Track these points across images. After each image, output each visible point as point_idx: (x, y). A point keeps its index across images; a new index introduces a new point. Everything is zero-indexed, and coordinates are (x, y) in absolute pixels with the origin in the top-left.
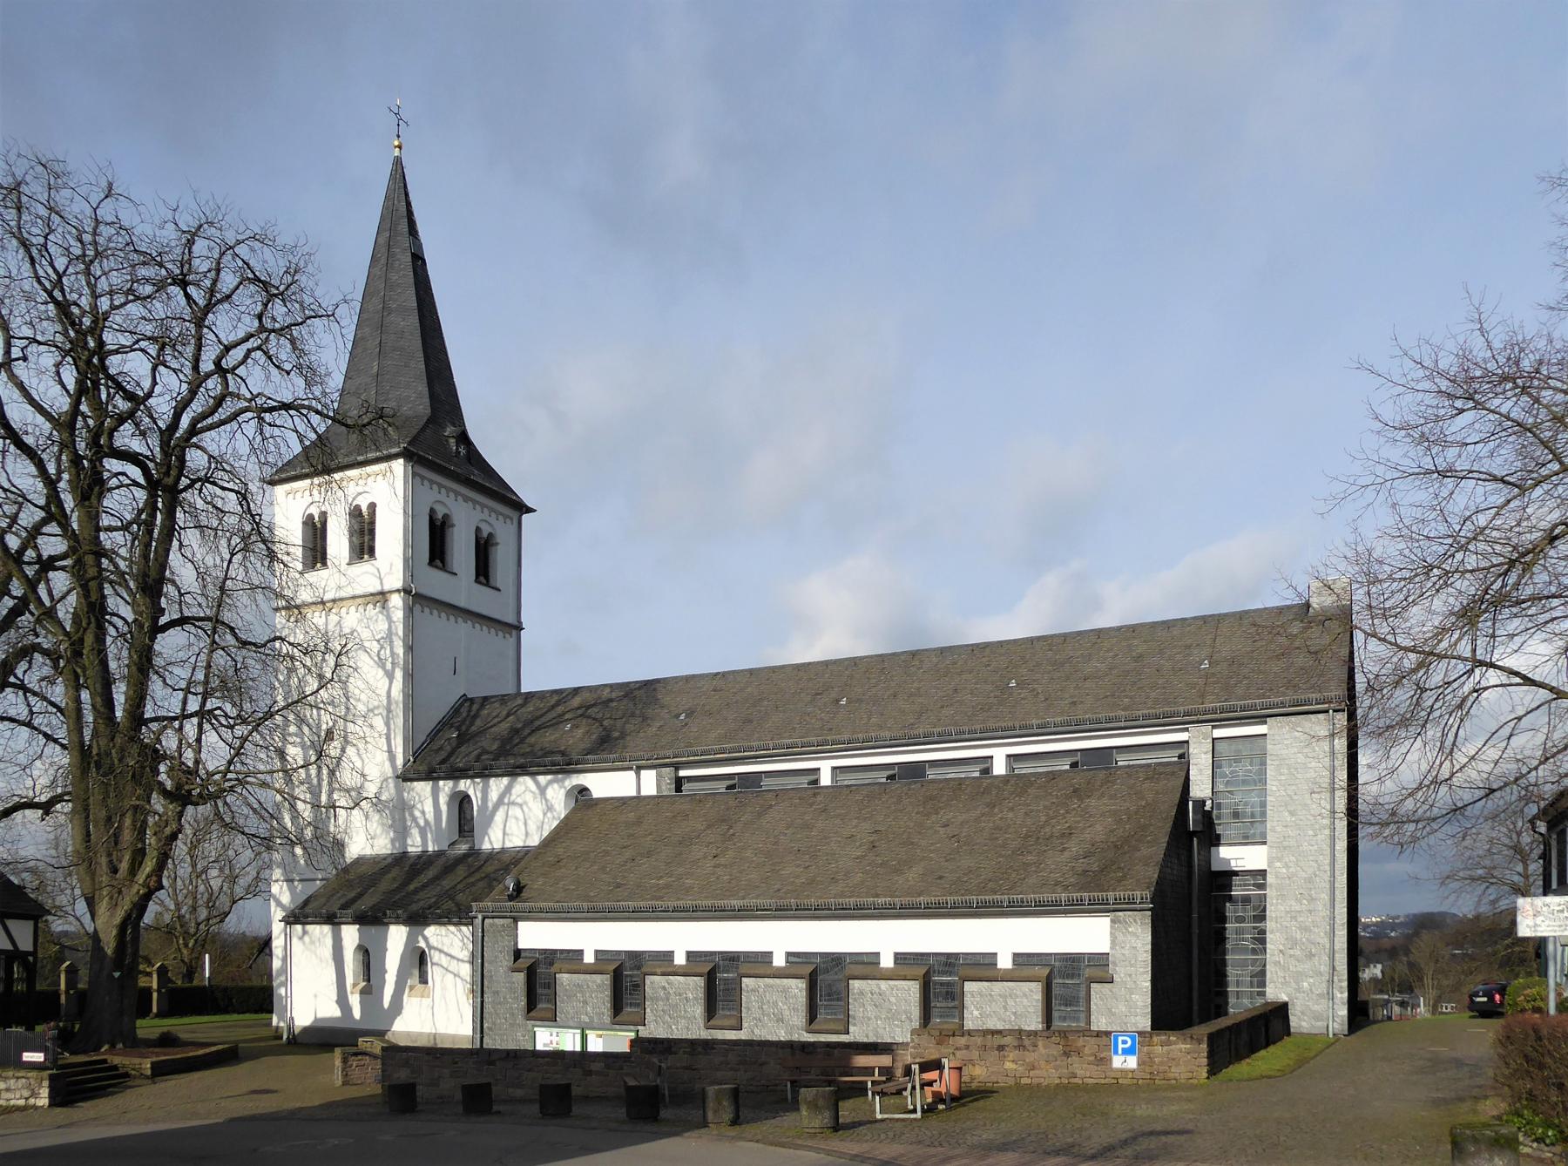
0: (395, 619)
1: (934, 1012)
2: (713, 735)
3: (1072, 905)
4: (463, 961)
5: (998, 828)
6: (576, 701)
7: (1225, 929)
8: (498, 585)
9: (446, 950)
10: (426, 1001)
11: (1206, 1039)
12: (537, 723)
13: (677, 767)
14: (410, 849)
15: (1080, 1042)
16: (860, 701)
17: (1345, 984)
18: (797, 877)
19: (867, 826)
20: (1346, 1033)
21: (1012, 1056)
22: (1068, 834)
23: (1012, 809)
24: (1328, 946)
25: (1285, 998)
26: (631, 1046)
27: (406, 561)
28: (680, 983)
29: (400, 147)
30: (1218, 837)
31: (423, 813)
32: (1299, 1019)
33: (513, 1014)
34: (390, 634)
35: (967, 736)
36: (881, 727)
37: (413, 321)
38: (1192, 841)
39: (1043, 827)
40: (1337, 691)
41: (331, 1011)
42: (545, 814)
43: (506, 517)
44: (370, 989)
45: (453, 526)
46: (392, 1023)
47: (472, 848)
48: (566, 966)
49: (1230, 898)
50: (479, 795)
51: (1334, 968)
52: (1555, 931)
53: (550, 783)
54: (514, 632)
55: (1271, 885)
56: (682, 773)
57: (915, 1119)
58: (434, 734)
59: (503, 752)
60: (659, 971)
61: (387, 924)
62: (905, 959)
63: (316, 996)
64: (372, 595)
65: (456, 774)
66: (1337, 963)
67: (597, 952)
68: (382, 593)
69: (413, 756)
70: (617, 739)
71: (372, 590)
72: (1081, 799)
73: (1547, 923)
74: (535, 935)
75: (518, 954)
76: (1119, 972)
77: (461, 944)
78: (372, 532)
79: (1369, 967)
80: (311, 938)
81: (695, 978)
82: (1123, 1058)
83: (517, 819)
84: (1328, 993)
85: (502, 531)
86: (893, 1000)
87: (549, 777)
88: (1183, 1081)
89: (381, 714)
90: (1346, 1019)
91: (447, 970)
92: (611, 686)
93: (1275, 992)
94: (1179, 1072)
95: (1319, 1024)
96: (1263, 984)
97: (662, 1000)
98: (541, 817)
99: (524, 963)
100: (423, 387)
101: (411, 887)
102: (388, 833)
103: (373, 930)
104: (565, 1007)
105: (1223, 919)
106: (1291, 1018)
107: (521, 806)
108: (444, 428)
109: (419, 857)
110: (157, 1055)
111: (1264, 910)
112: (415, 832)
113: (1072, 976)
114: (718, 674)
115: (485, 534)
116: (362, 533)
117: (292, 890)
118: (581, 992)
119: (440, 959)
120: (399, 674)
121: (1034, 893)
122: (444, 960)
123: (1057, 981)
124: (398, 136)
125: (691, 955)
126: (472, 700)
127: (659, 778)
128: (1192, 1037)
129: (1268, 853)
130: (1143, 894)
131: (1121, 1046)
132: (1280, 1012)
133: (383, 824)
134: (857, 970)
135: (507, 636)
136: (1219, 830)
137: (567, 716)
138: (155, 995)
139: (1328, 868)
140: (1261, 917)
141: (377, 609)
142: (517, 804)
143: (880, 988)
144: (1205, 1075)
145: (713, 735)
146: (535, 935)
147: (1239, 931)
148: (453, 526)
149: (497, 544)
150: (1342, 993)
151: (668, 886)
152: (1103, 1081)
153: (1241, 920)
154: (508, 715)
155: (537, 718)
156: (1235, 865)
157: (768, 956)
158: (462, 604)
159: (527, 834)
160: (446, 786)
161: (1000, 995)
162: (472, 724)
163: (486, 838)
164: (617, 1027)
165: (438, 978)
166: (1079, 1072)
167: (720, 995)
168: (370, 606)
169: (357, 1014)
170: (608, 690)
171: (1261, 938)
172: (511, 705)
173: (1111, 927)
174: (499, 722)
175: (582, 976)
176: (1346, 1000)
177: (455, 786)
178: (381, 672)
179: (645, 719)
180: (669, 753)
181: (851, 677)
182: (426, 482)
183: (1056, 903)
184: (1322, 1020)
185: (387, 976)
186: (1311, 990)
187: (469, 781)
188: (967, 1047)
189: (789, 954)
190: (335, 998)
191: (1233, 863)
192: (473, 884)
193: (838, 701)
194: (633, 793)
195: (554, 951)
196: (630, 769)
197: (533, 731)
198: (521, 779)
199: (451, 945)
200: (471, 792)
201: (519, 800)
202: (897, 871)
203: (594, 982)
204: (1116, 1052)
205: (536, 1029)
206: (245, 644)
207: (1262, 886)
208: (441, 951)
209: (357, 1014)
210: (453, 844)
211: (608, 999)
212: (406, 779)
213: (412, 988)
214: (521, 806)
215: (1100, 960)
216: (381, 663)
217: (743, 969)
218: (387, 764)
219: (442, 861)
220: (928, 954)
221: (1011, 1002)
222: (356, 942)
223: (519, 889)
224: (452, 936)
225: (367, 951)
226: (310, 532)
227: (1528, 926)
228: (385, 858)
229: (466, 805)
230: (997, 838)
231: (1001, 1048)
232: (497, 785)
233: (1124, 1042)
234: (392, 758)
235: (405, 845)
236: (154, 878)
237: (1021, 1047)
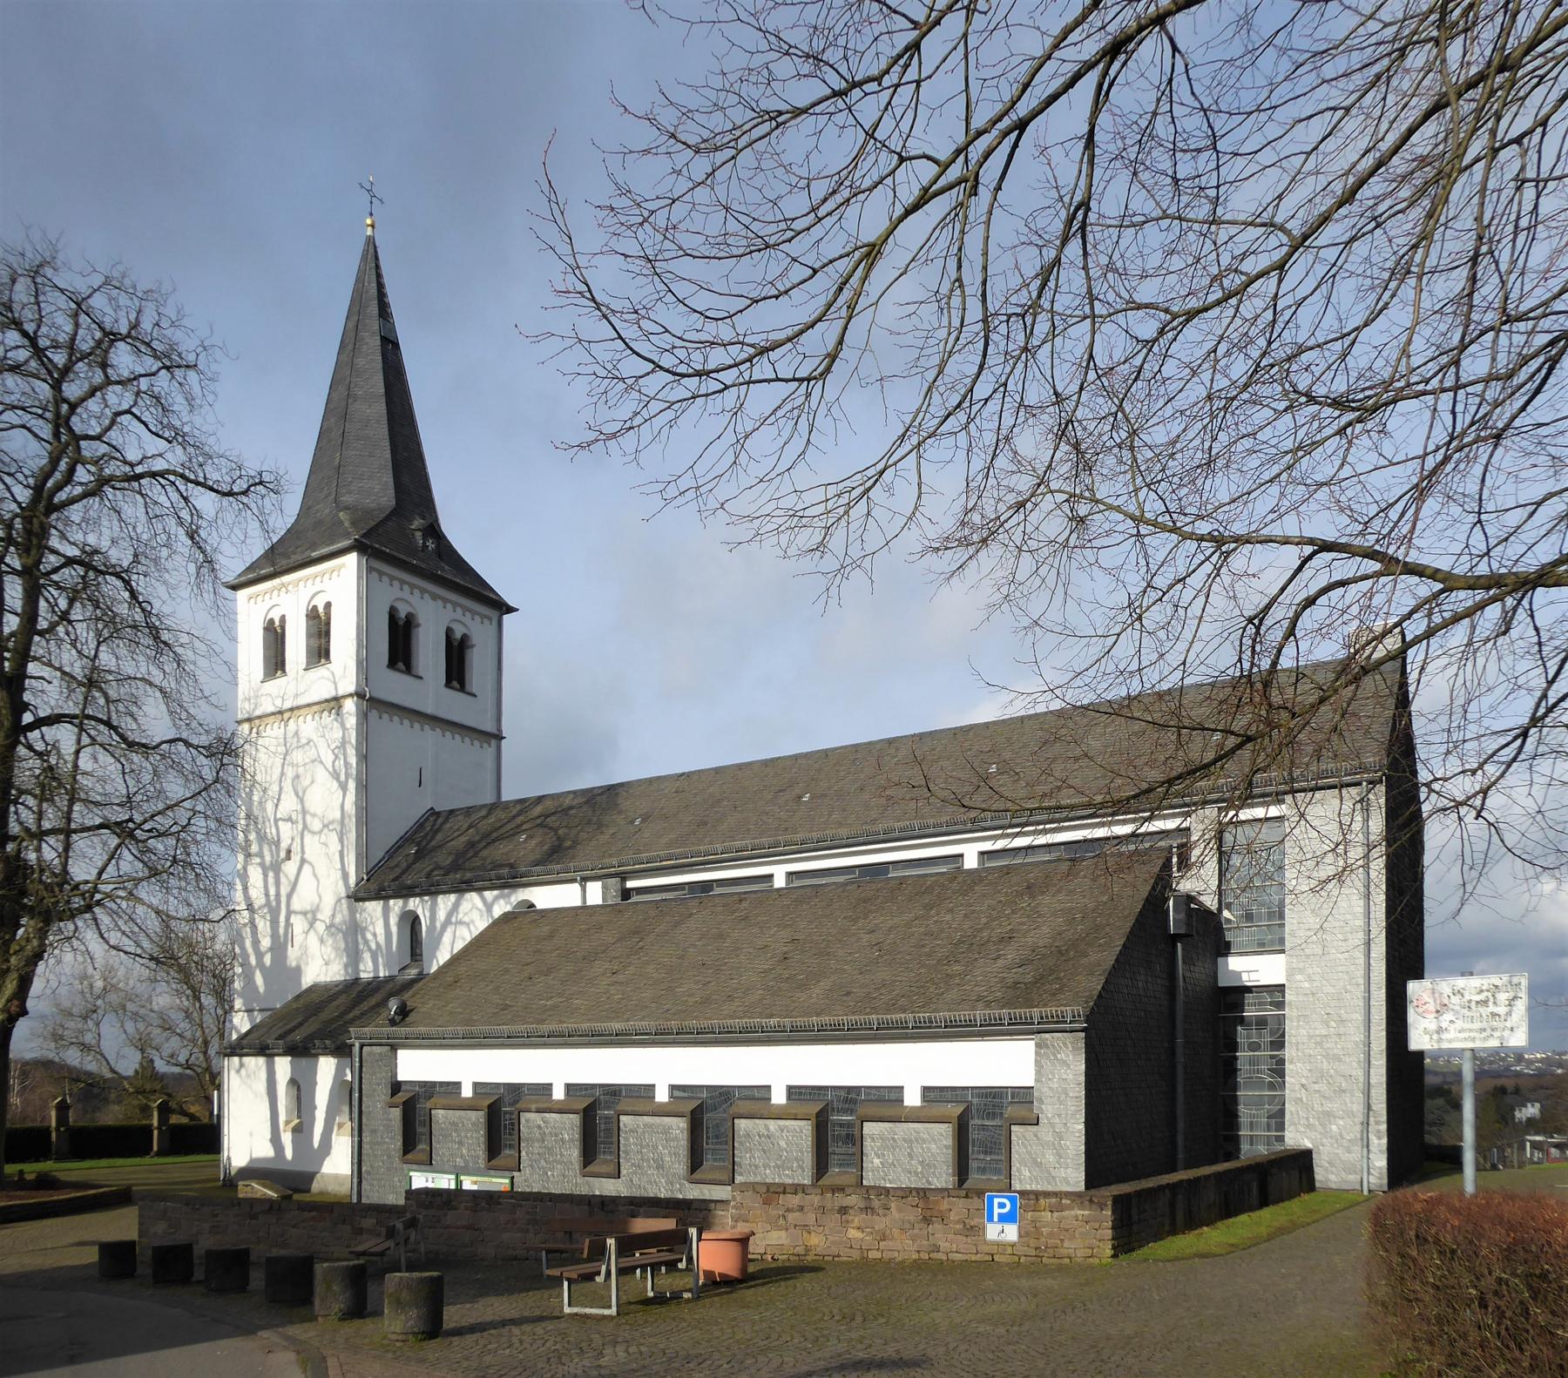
0: (348, 726)
1: (833, 1159)
2: (664, 840)
3: (990, 1025)
5: (930, 934)
6: (538, 810)
7: (1236, 1058)
8: (474, 691)
11: (1110, 1203)
12: (495, 835)
13: (624, 877)
14: (363, 975)
15: (945, 1205)
16: (824, 796)
17: (1384, 1127)
18: (692, 995)
19: (785, 934)
20: (1386, 1189)
21: (857, 1220)
22: (1009, 938)
23: (951, 911)
24: (1361, 1080)
25: (1309, 1145)
26: (406, 1198)
27: (359, 663)
28: (555, 1121)
29: (373, 226)
30: (1228, 945)
31: (375, 935)
32: (1326, 1170)
33: (389, 1156)
34: (344, 743)
35: (931, 830)
36: (840, 825)
37: (380, 408)
38: (1175, 947)
39: (981, 930)
40: (1374, 756)
41: (265, 1151)
43: (483, 617)
44: (301, 1131)
45: (418, 625)
47: (421, 973)
48: (445, 1101)
49: (1242, 1020)
50: (428, 914)
51: (1369, 1108)
52: (1473, 1040)
53: (496, 898)
54: (493, 742)
55: (1290, 1003)
56: (630, 884)
57: (604, 1317)
58: (392, 852)
59: (455, 867)
60: (533, 1107)
61: (316, 1056)
62: (800, 1093)
63: (251, 1134)
64: (327, 701)
65: (405, 892)
66: (1373, 1101)
67: (476, 1085)
68: (336, 699)
70: (569, 848)
71: (328, 696)
72: (1033, 897)
73: (1459, 1024)
74: (415, 1065)
75: (396, 1087)
76: (1047, 1110)
78: (328, 633)
79: (1526, 1106)
81: (571, 1116)
82: (999, 1227)
84: (1362, 1139)
85: (476, 629)
86: (783, 1144)
87: (496, 892)
88: (1079, 1260)
90: (1385, 1171)
92: (574, 792)
93: (1296, 1137)
94: (1075, 1248)
95: (1351, 1177)
96: (1281, 1127)
97: (538, 1140)
99: (402, 1097)
100: (388, 478)
103: (304, 1062)
104: (441, 1150)
105: (1234, 1047)
106: (1316, 1169)
107: (468, 925)
108: (410, 521)
109: (369, 983)
110: (21, 1198)
111: (1283, 1035)
112: (367, 956)
113: (992, 1116)
114: (683, 774)
115: (458, 635)
116: (320, 635)
117: (251, 1019)
118: (456, 1131)
120: (352, 785)
121: (949, 1010)
123: (975, 1122)
124: (371, 214)
125: (792, 1091)
126: (438, 814)
127: (605, 888)
128: (1091, 1201)
129: (1287, 962)
130: (1074, 1010)
131: (997, 1211)
132: (1302, 1161)
134: (743, 1106)
135: (485, 745)
136: (1229, 937)
137: (524, 827)
138: (156, 1133)
139: (1361, 981)
140: (1279, 1044)
141: (333, 717)
143: (768, 1130)
144: (1109, 1252)
145: (664, 840)
146: (415, 1065)
147: (1253, 1062)
148: (418, 625)
149: (473, 646)
150: (1379, 1138)
151: (555, 1007)
152: (974, 1258)
153: (1255, 1047)
154: (470, 827)
155: (496, 829)
156: (1248, 980)
157: (457, 1085)
158: (429, 710)
160: (396, 905)
161: (904, 1140)
162: (433, 838)
164: (492, 1172)
166: (944, 1245)
167: (601, 1137)
168: (326, 714)
169: (289, 1154)
170: (571, 796)
171: (1279, 1070)
172: (475, 817)
173: (1036, 1053)
175: (458, 1113)
176: (1385, 1147)
177: (405, 904)
178: (335, 784)
179: (600, 825)
180: (615, 862)
181: (819, 770)
182: (385, 579)
183: (971, 1023)
184: (1356, 1173)
186: (1341, 1135)
188: (801, 1209)
189: (673, 1088)
190: (269, 1137)
191: (1245, 977)
193: (800, 797)
194: (578, 903)
195: (433, 1084)
196: (573, 881)
197: (489, 844)
200: (420, 912)
201: (466, 919)
202: (803, 986)
203: (470, 1119)
204: (991, 1219)
205: (411, 1174)
206: (131, 745)
207: (1280, 1005)
209: (289, 1154)
210: (404, 968)
211: (482, 1139)
212: (358, 900)
213: (340, 1126)
215: (1023, 1095)
216: (335, 775)
217: (862, 1110)
218: (341, 883)
219: (390, 986)
220: (826, 1088)
221: (917, 1149)
222: (288, 1076)
223: (404, 1012)
226: (272, 638)
227: (1426, 1031)
228: (337, 984)
230: (923, 946)
231: (843, 1210)
232: (445, 902)
233: (1002, 1206)
234: (345, 876)
235: (357, 970)
236: (16, 1002)
237: (868, 1209)
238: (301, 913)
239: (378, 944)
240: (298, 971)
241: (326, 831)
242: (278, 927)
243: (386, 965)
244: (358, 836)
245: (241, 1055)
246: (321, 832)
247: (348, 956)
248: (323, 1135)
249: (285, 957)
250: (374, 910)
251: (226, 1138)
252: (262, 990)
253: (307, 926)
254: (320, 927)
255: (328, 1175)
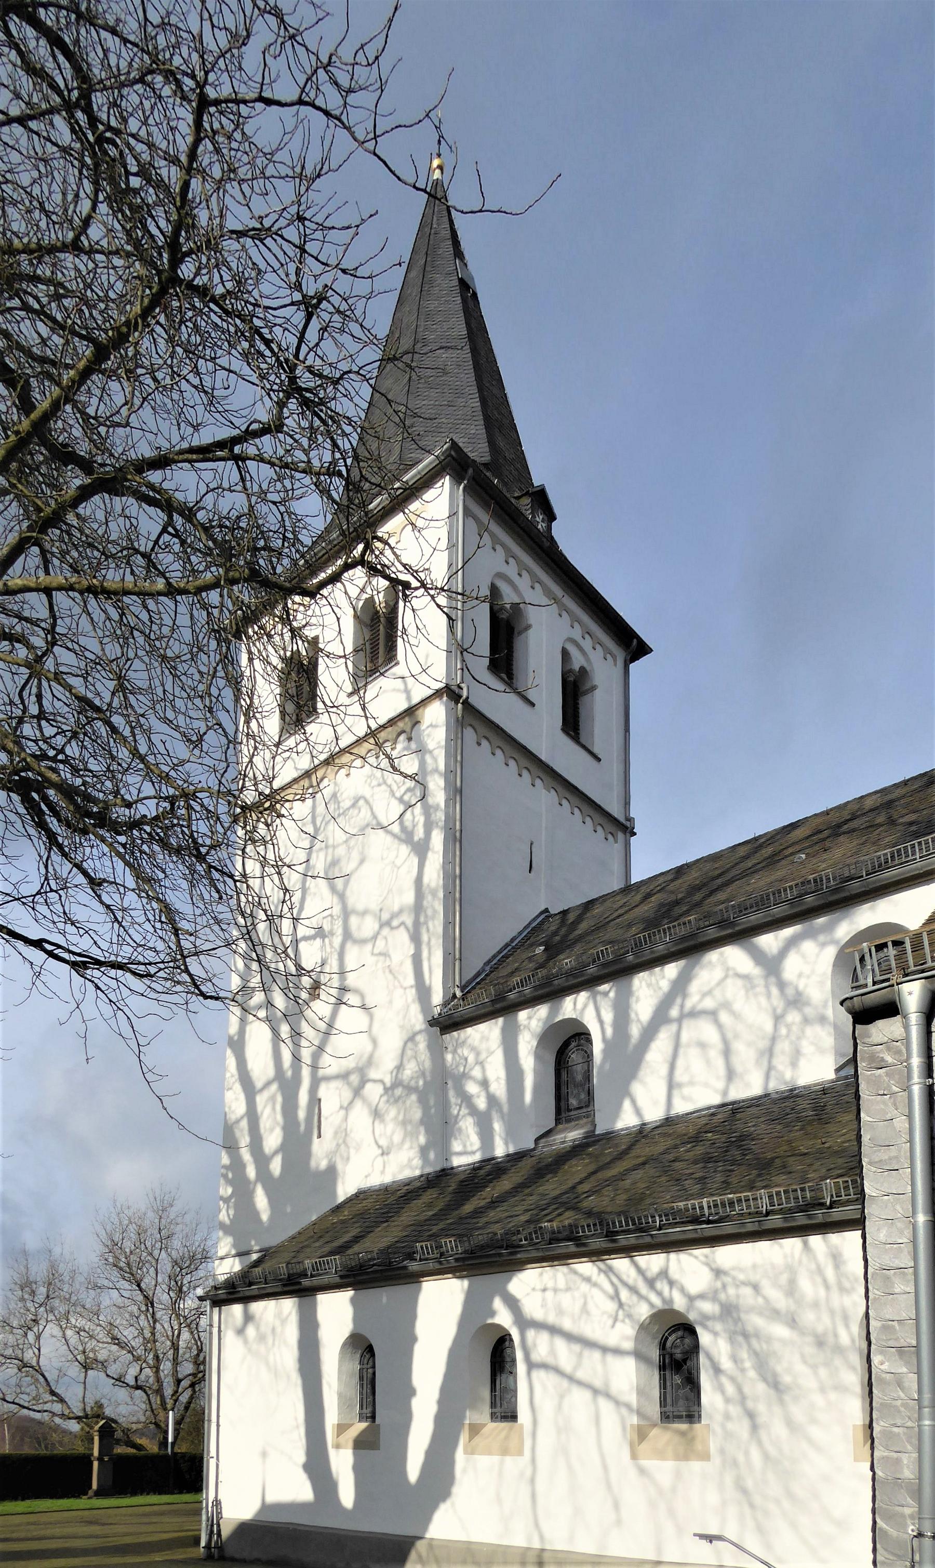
4: (617, 1352)
9: (567, 1324)
10: (514, 1465)
29: (440, 167)
31: (485, 1084)
42: (778, 1019)
43: (607, 651)
46: (426, 1520)
54: (620, 836)
61: (415, 1278)
63: (264, 1454)
69: (462, 988)
77: (611, 1306)
80: (258, 1328)
83: (702, 1045)
87: (788, 932)
89: (403, 923)
91: (571, 1378)
98: (769, 1026)
101: (468, 1208)
102: (414, 1135)
103: (384, 1296)
107: (713, 1014)
112: (468, 1125)
119: (552, 1352)
122: (564, 1355)
133: (404, 1123)
138: (96, 1464)
142: (704, 1012)
159: (731, 1075)
163: (627, 1104)
165: (546, 1406)
169: (347, 1496)
174: (626, 912)
177: (553, 1012)
178: (405, 850)
185: (415, 1403)
187: (583, 996)
192: (622, 1176)
198: (713, 956)
199: (585, 1309)
201: (708, 1004)
208: (554, 1330)
209: (347, 1496)
213: (475, 1430)
214: (713, 1014)
224: (585, 1287)
225: (370, 1350)
228: (409, 1182)
229: (575, 1057)
235: (445, 1151)
238: (337, 1077)
239: (492, 1100)
240: (331, 1174)
241: (386, 931)
242: (295, 1106)
243: (510, 1134)
244: (448, 923)
245: (246, 1300)
246: (375, 938)
247: (427, 1131)
248: (431, 1453)
249: (308, 1154)
250: (485, 1038)
251: (213, 1463)
252: (265, 1217)
253: (347, 1094)
254: (373, 1092)
255: (448, 1545)
